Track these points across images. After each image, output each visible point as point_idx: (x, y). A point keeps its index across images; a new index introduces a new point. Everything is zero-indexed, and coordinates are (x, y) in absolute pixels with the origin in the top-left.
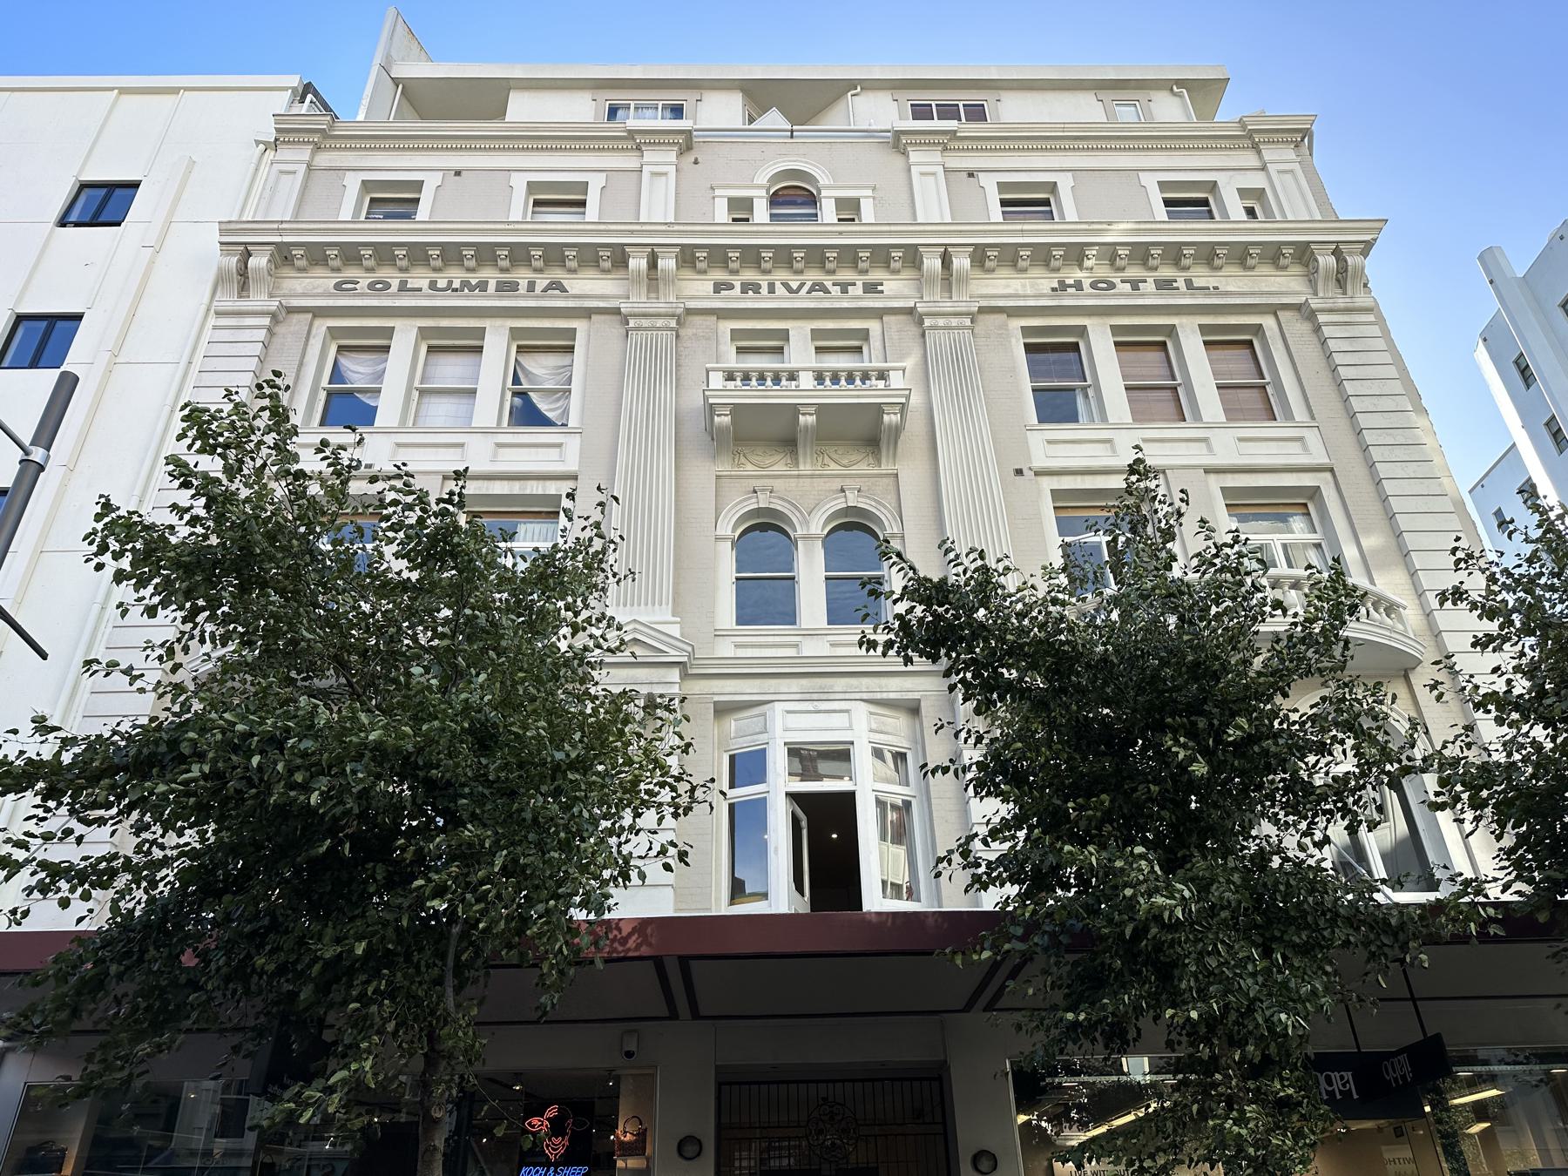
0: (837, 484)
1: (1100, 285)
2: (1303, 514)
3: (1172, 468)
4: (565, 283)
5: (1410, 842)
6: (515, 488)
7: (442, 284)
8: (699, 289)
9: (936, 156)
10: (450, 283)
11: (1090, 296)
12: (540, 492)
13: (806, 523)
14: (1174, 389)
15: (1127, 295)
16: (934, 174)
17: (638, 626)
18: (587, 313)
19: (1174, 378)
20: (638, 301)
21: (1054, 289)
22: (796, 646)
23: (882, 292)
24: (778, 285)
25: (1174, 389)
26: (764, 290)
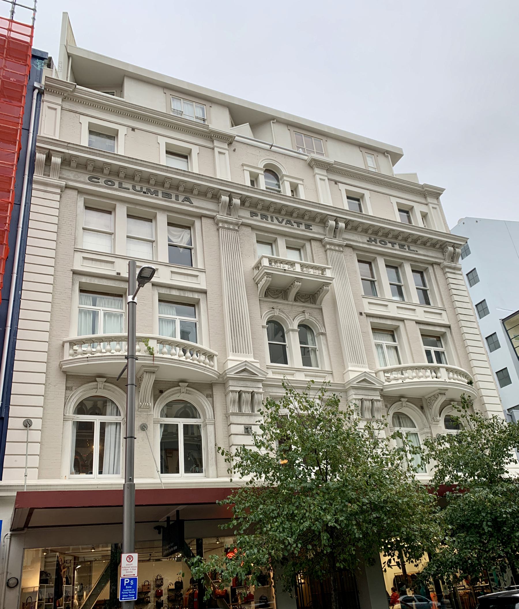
0: (301, 309)
1: (384, 243)
2: (391, 335)
3: (407, 319)
4: (191, 199)
5: (15, 498)
6: (182, 294)
7: (138, 188)
8: (245, 215)
9: (59, 100)
10: (141, 188)
11: (407, 252)
12: (191, 296)
13: (291, 324)
14: (191, 249)
15: (391, 249)
16: (55, 109)
17: (247, 364)
18: (201, 217)
19: (373, 277)
20: (221, 216)
21: (368, 241)
22: (325, 377)
23: (311, 229)
24: (274, 218)
25: (191, 249)
26: (269, 219)
